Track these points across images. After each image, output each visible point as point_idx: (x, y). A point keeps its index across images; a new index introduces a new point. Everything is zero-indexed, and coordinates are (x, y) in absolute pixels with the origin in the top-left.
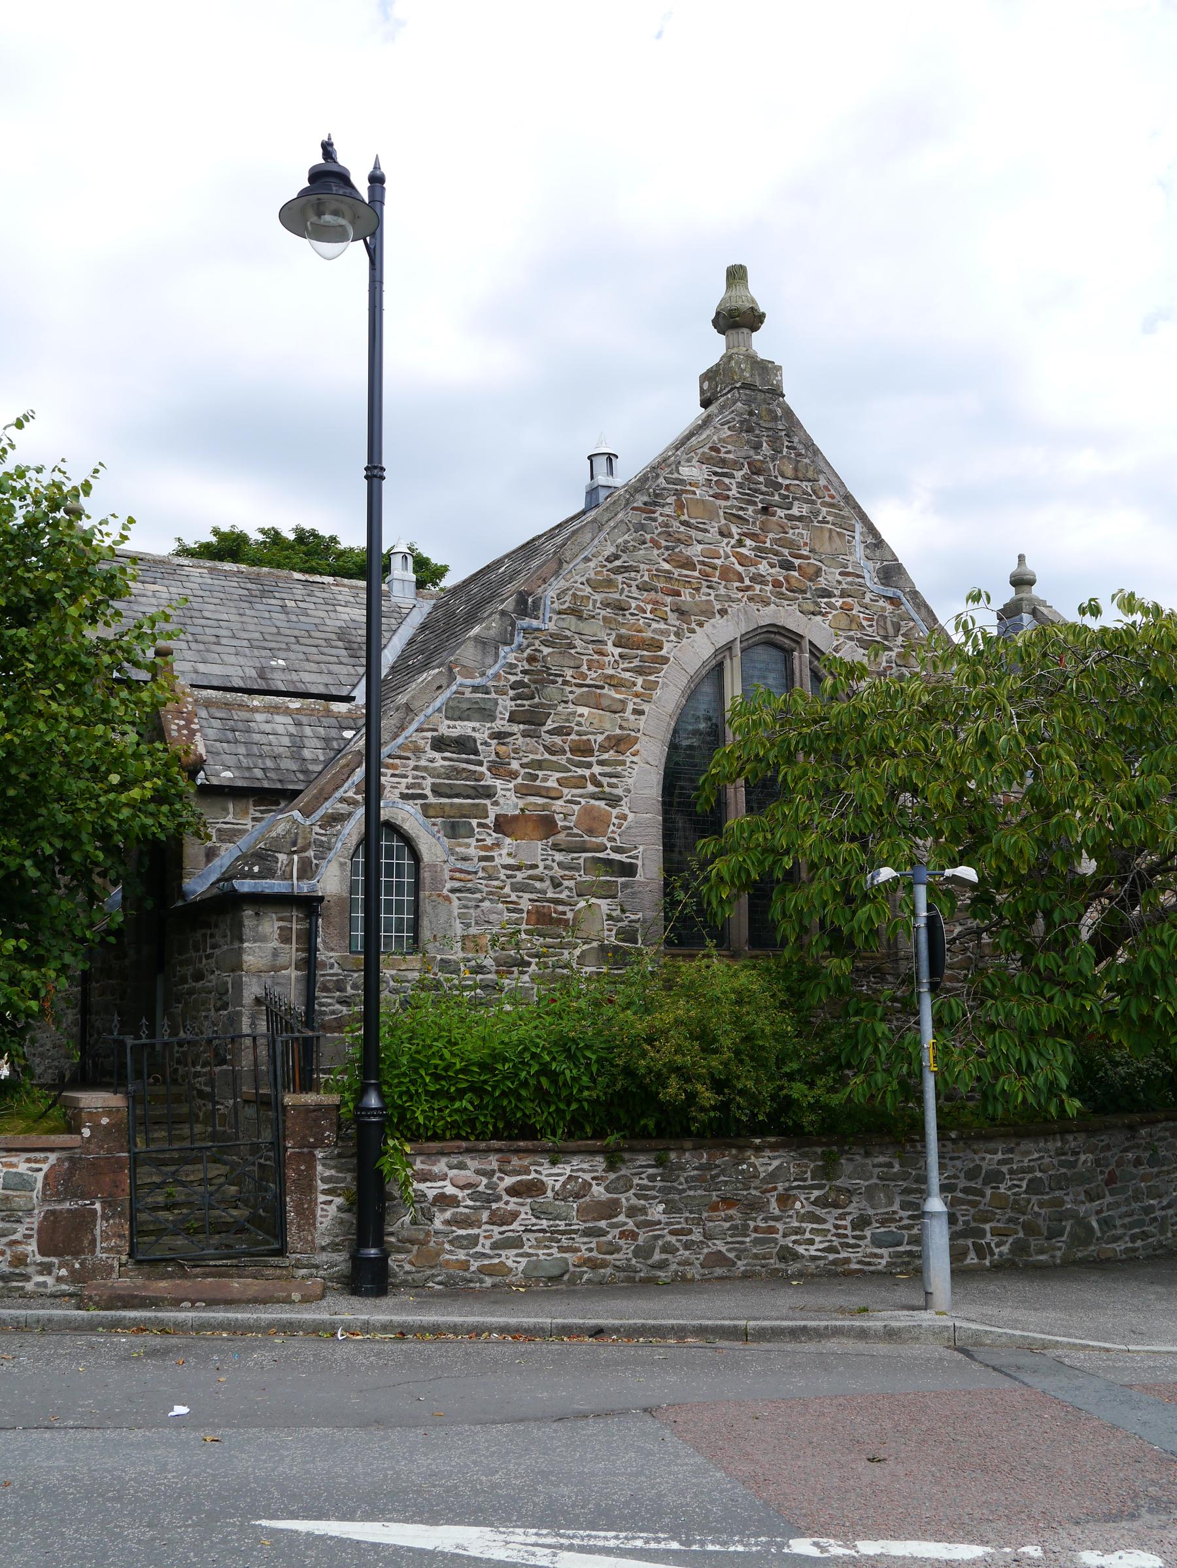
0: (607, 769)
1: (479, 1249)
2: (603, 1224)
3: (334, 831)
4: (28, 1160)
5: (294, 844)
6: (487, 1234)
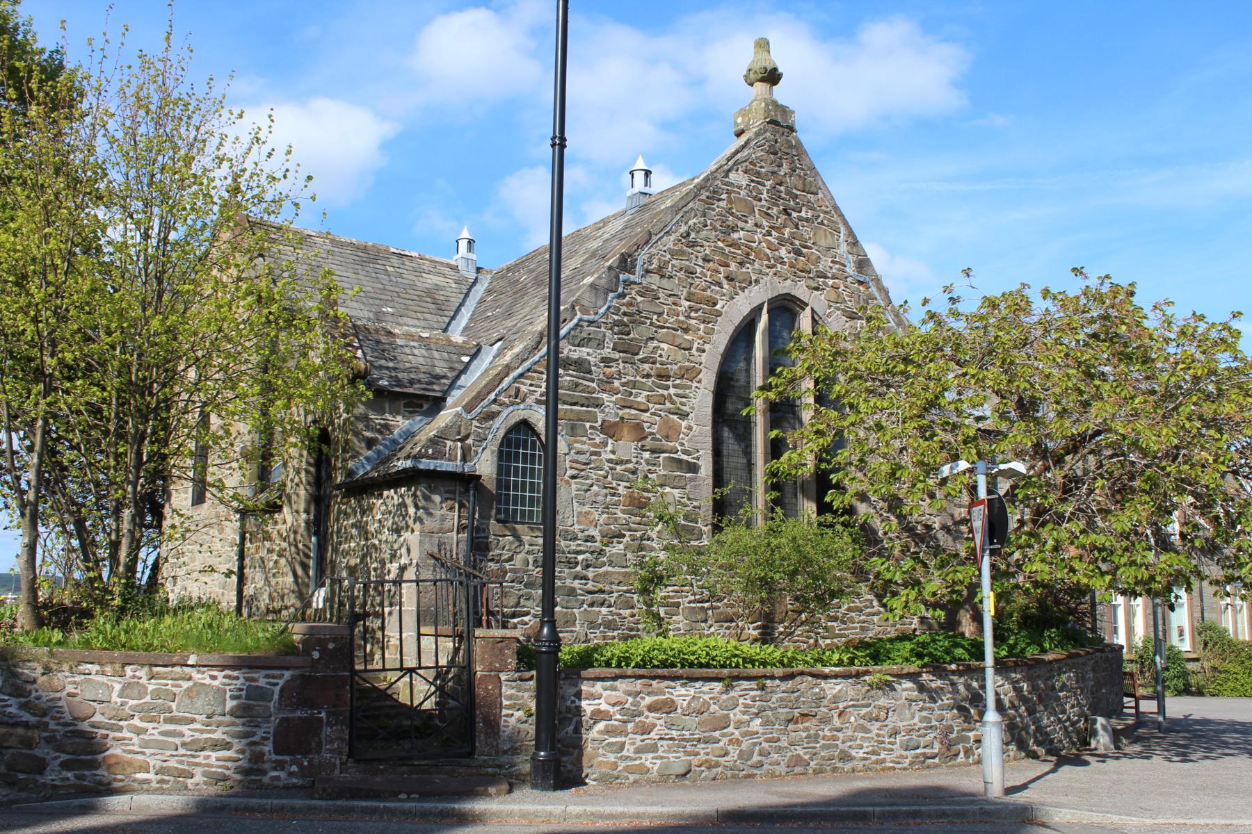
0: (680, 392)
1: (625, 753)
2: (717, 734)
3: (488, 425)
4: (267, 676)
5: (459, 433)
6: (632, 742)
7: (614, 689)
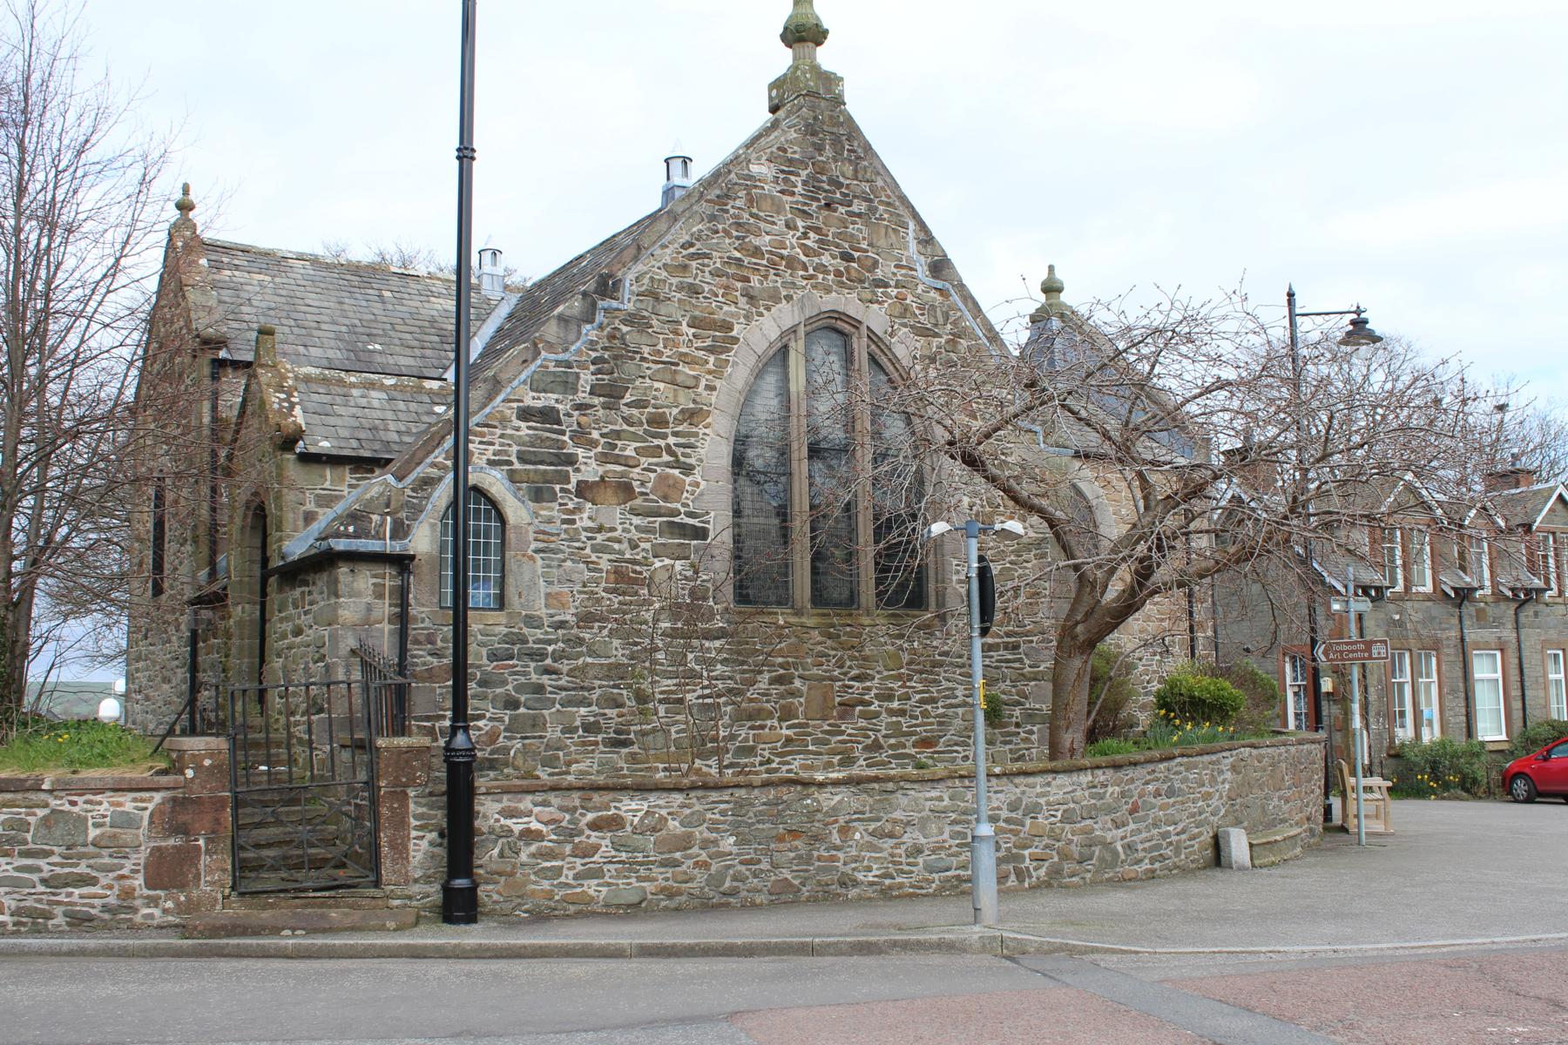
1: (563, 879)
2: (678, 855)
4: (135, 800)
5: (388, 506)
7: (545, 804)
